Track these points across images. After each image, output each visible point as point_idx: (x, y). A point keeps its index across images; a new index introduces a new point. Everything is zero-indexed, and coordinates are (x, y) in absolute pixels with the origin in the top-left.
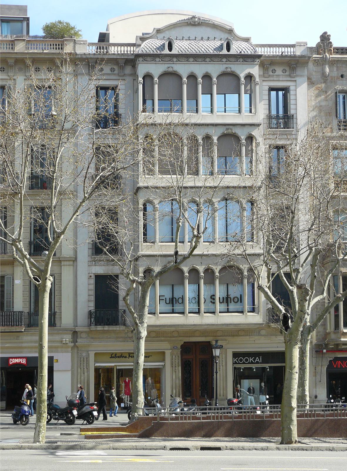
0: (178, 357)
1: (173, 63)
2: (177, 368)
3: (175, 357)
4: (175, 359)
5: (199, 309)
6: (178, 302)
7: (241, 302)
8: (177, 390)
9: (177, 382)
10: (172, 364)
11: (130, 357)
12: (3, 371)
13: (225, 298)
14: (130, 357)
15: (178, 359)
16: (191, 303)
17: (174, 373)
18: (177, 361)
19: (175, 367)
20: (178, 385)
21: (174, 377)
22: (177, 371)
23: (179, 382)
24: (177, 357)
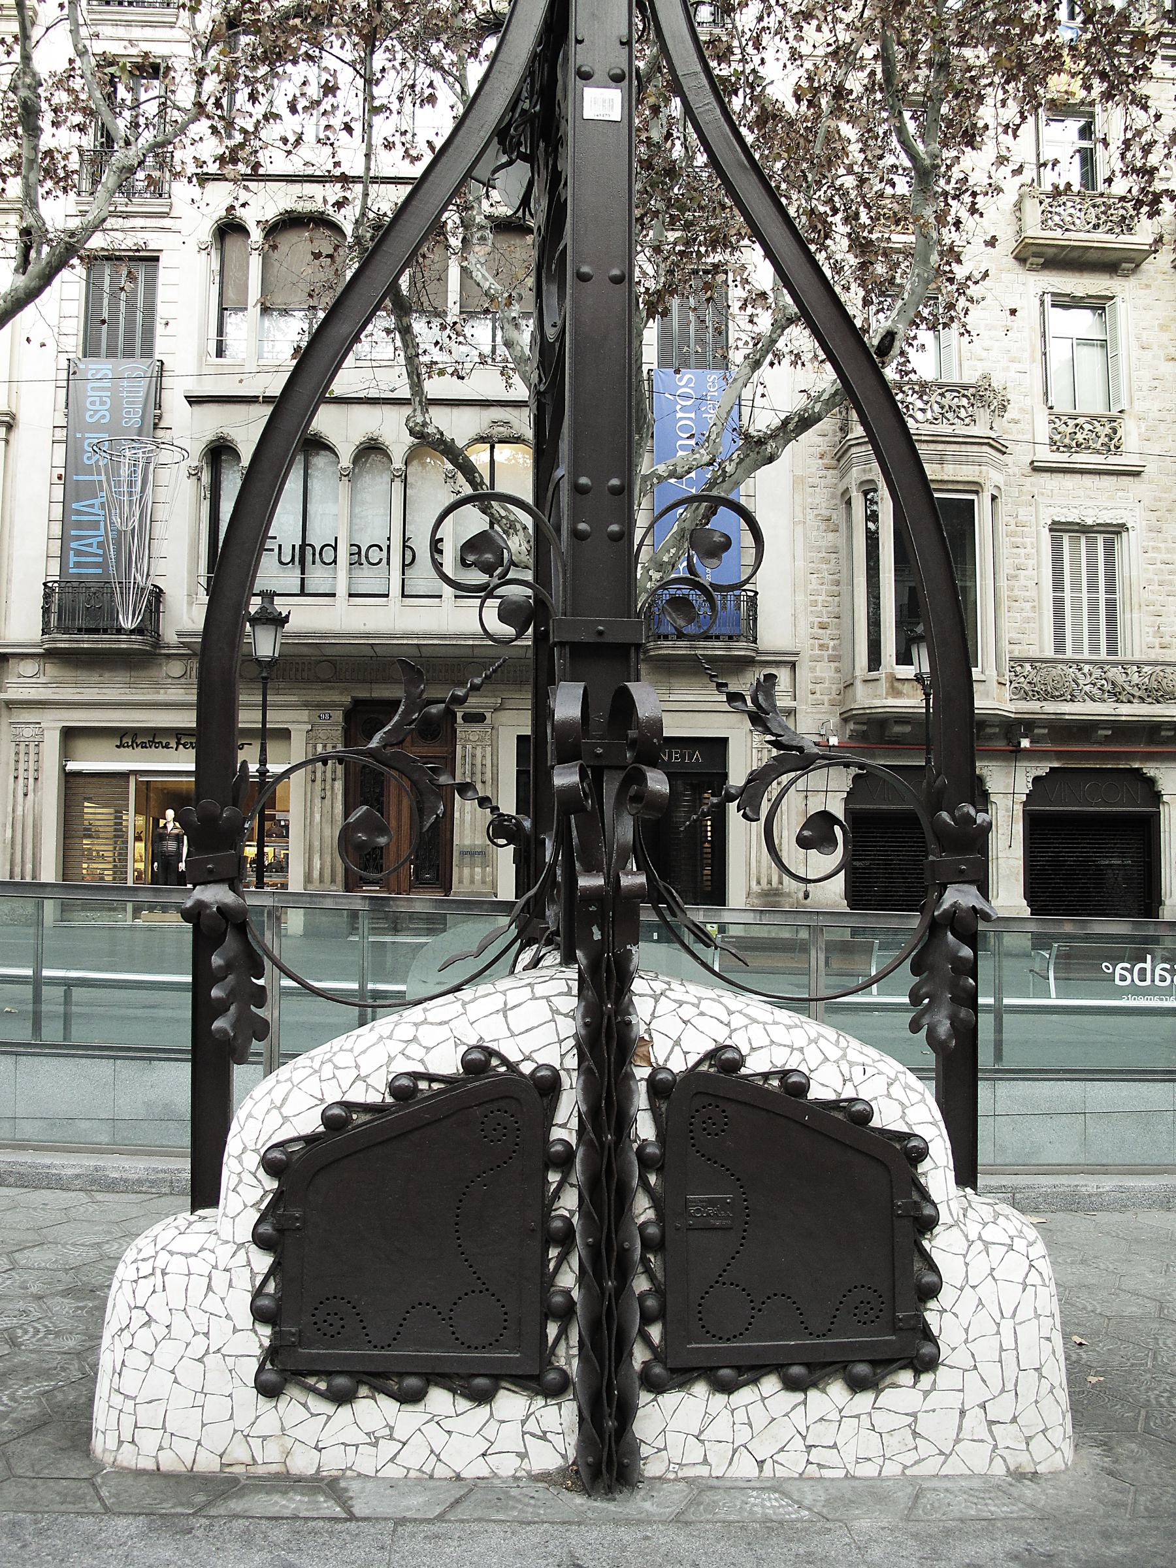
9: (327, 832)
17: (318, 801)
21: (317, 817)
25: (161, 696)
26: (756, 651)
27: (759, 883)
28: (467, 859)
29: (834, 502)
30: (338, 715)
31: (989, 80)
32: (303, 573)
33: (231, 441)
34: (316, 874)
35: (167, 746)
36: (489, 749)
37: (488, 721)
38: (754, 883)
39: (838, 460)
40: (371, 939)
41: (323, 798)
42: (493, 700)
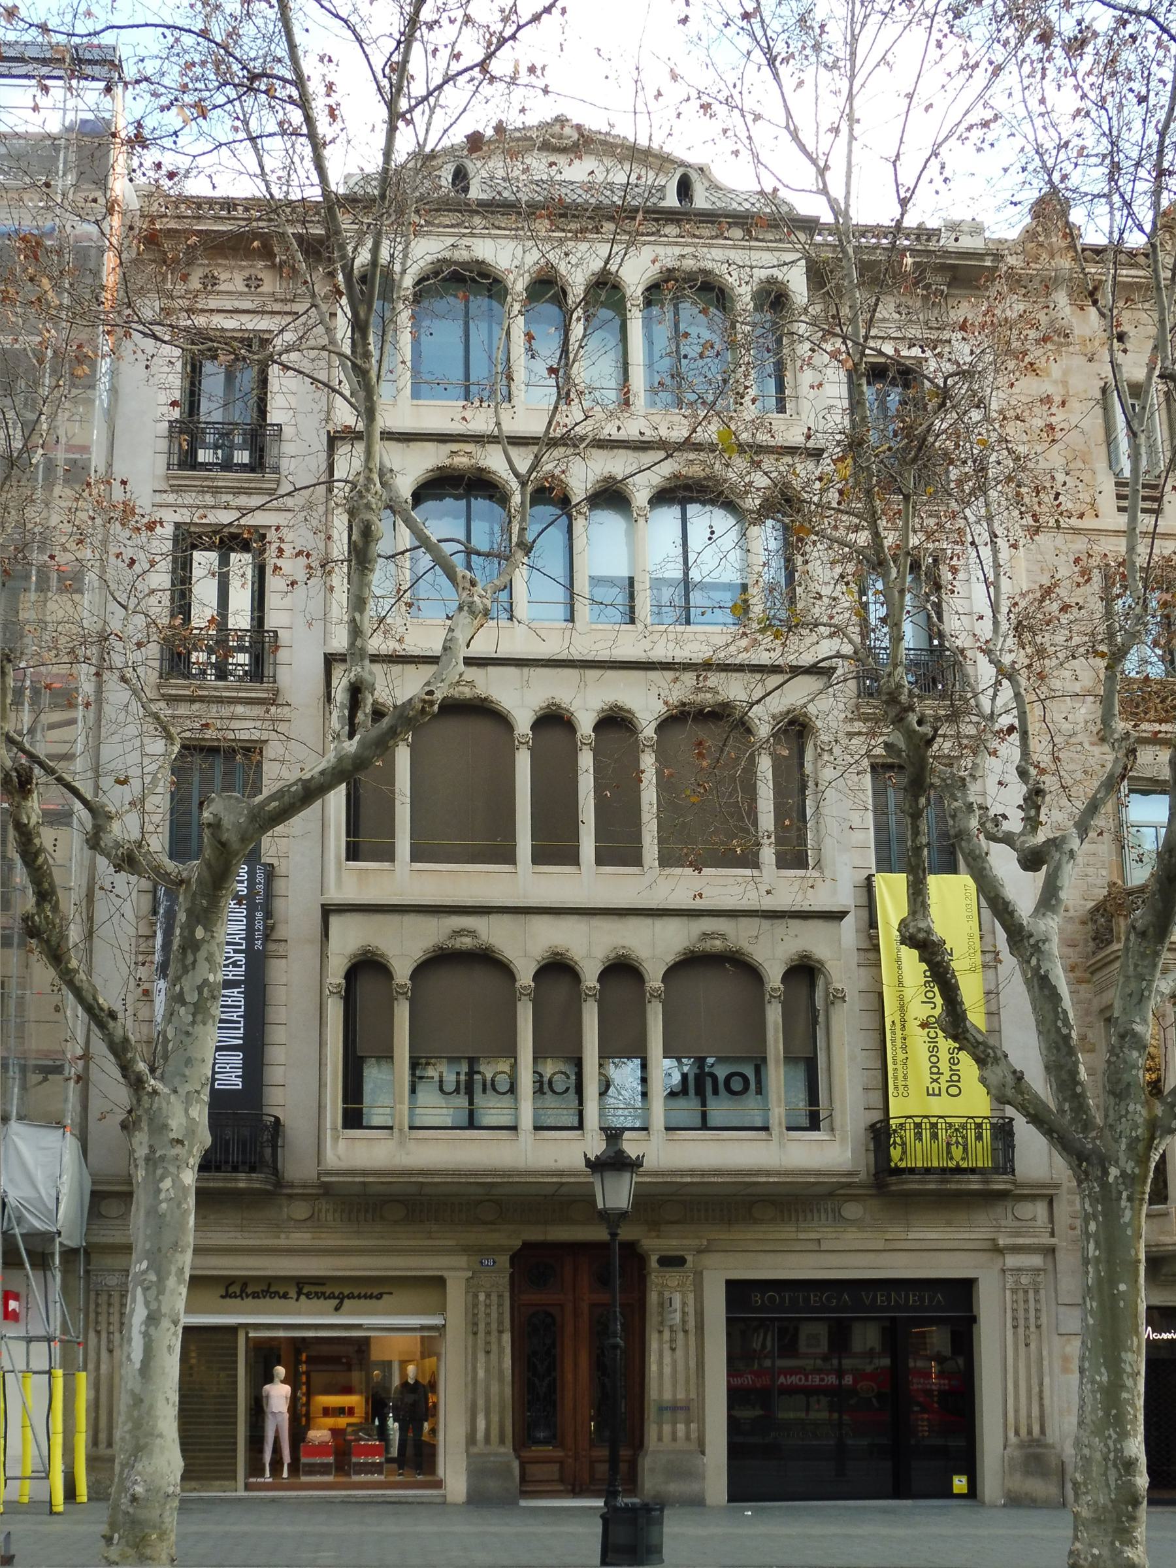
0: (500, 1296)
1: (473, 235)
2: (493, 1338)
3: (488, 1296)
4: (488, 1306)
5: (581, 1114)
6: (494, 1089)
7: (759, 1091)
8: (495, 1418)
9: (495, 1388)
10: (476, 1324)
11: (303, 1297)
12: (193, 1347)
13: (691, 1078)
14: (303, 1297)
15: (500, 1305)
16: (549, 1095)
17: (481, 1357)
18: (494, 1315)
19: (97, 1314)
20: (495, 1399)
21: (481, 1374)
22: (494, 1347)
23: (502, 1390)
24: (494, 1298)
25: (282, 1241)
26: (1014, 1183)
27: (1017, 1433)
28: (667, 1415)
29: (1089, 1019)
30: (504, 1261)
31: (342, 288)
32: (471, 1102)
33: (382, 955)
34: (480, 1434)
35: (285, 1296)
36: (691, 1296)
37: (689, 1264)
38: (1011, 1434)
39: (1092, 973)
40: (285, 1475)
41: (488, 1352)
42: (697, 1242)
